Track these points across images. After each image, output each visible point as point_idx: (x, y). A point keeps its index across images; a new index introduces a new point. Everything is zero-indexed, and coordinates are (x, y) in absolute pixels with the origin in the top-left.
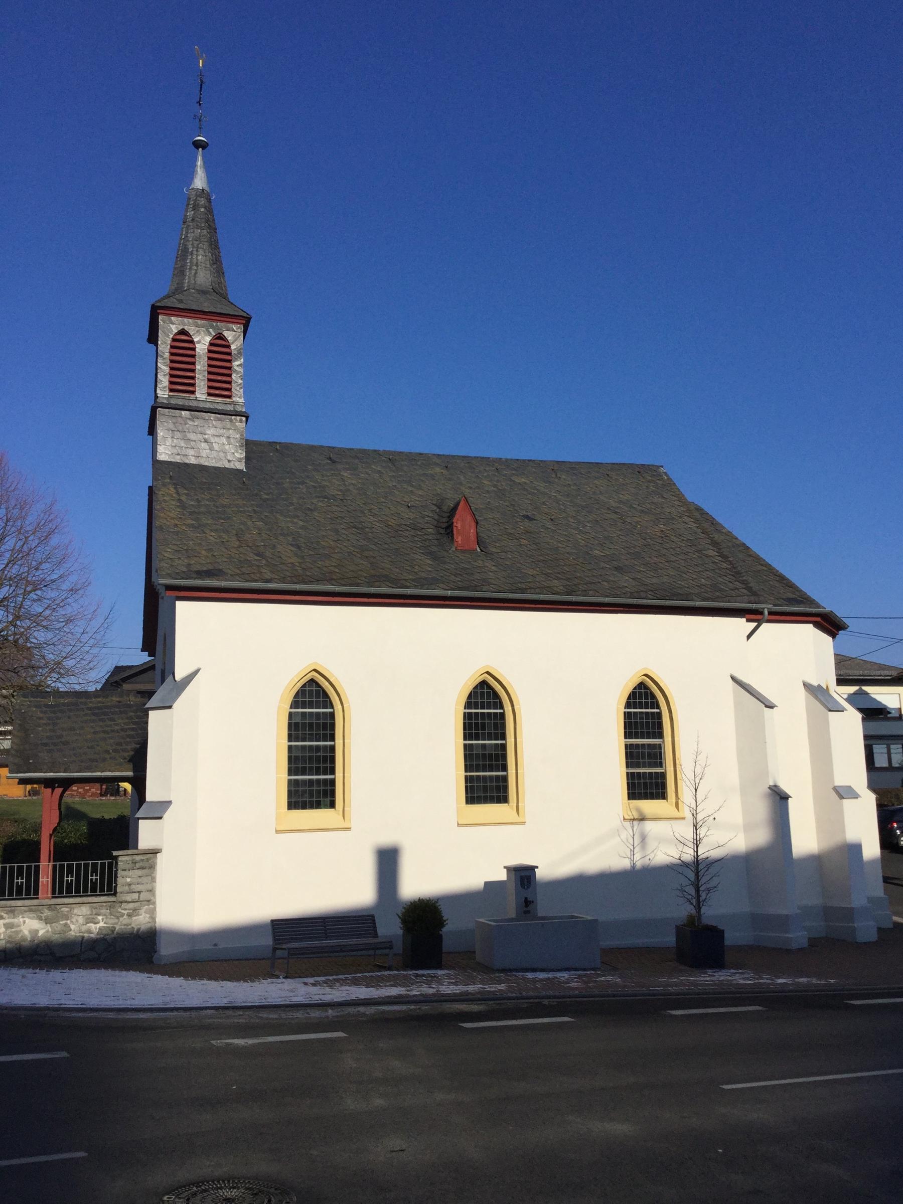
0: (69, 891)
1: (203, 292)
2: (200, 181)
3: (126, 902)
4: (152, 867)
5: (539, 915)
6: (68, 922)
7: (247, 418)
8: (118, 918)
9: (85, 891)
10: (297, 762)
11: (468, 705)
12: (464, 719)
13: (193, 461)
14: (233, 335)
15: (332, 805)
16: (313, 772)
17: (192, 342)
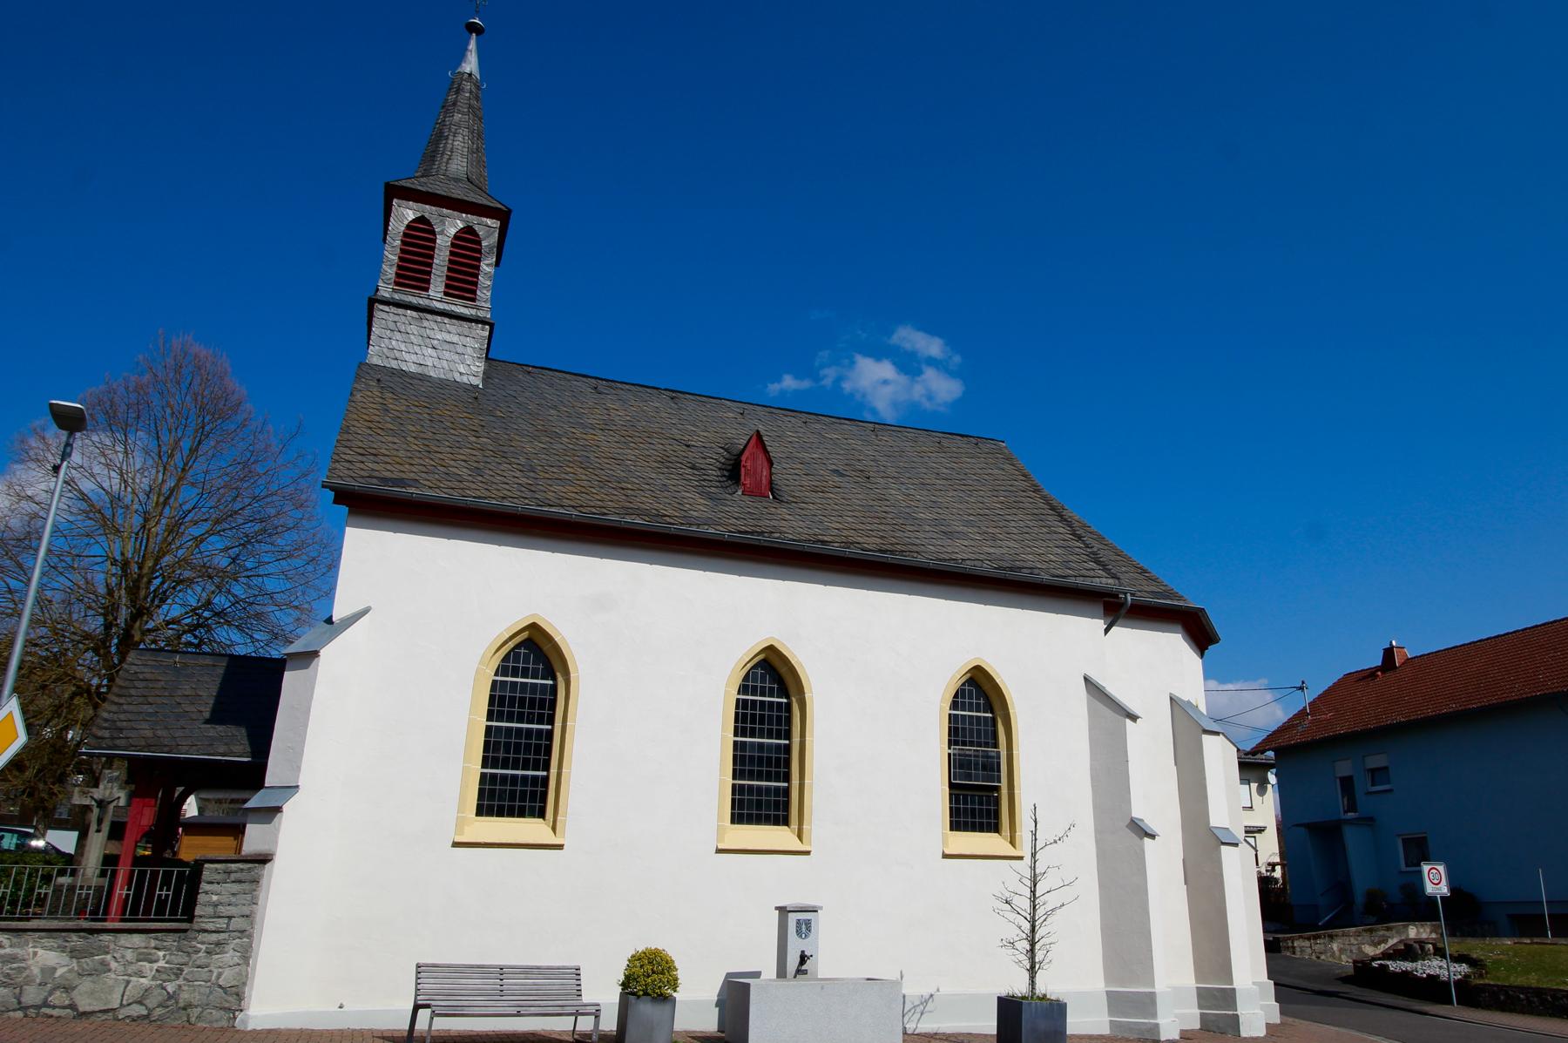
0: (161, 910)
1: (457, 180)
2: (471, 65)
3: (206, 931)
4: (256, 882)
6: (109, 957)
7: (492, 326)
8: (189, 954)
9: (147, 911)
10: (496, 749)
11: (743, 689)
12: (737, 707)
13: (413, 369)
14: (487, 229)
16: (519, 762)
17: (433, 233)
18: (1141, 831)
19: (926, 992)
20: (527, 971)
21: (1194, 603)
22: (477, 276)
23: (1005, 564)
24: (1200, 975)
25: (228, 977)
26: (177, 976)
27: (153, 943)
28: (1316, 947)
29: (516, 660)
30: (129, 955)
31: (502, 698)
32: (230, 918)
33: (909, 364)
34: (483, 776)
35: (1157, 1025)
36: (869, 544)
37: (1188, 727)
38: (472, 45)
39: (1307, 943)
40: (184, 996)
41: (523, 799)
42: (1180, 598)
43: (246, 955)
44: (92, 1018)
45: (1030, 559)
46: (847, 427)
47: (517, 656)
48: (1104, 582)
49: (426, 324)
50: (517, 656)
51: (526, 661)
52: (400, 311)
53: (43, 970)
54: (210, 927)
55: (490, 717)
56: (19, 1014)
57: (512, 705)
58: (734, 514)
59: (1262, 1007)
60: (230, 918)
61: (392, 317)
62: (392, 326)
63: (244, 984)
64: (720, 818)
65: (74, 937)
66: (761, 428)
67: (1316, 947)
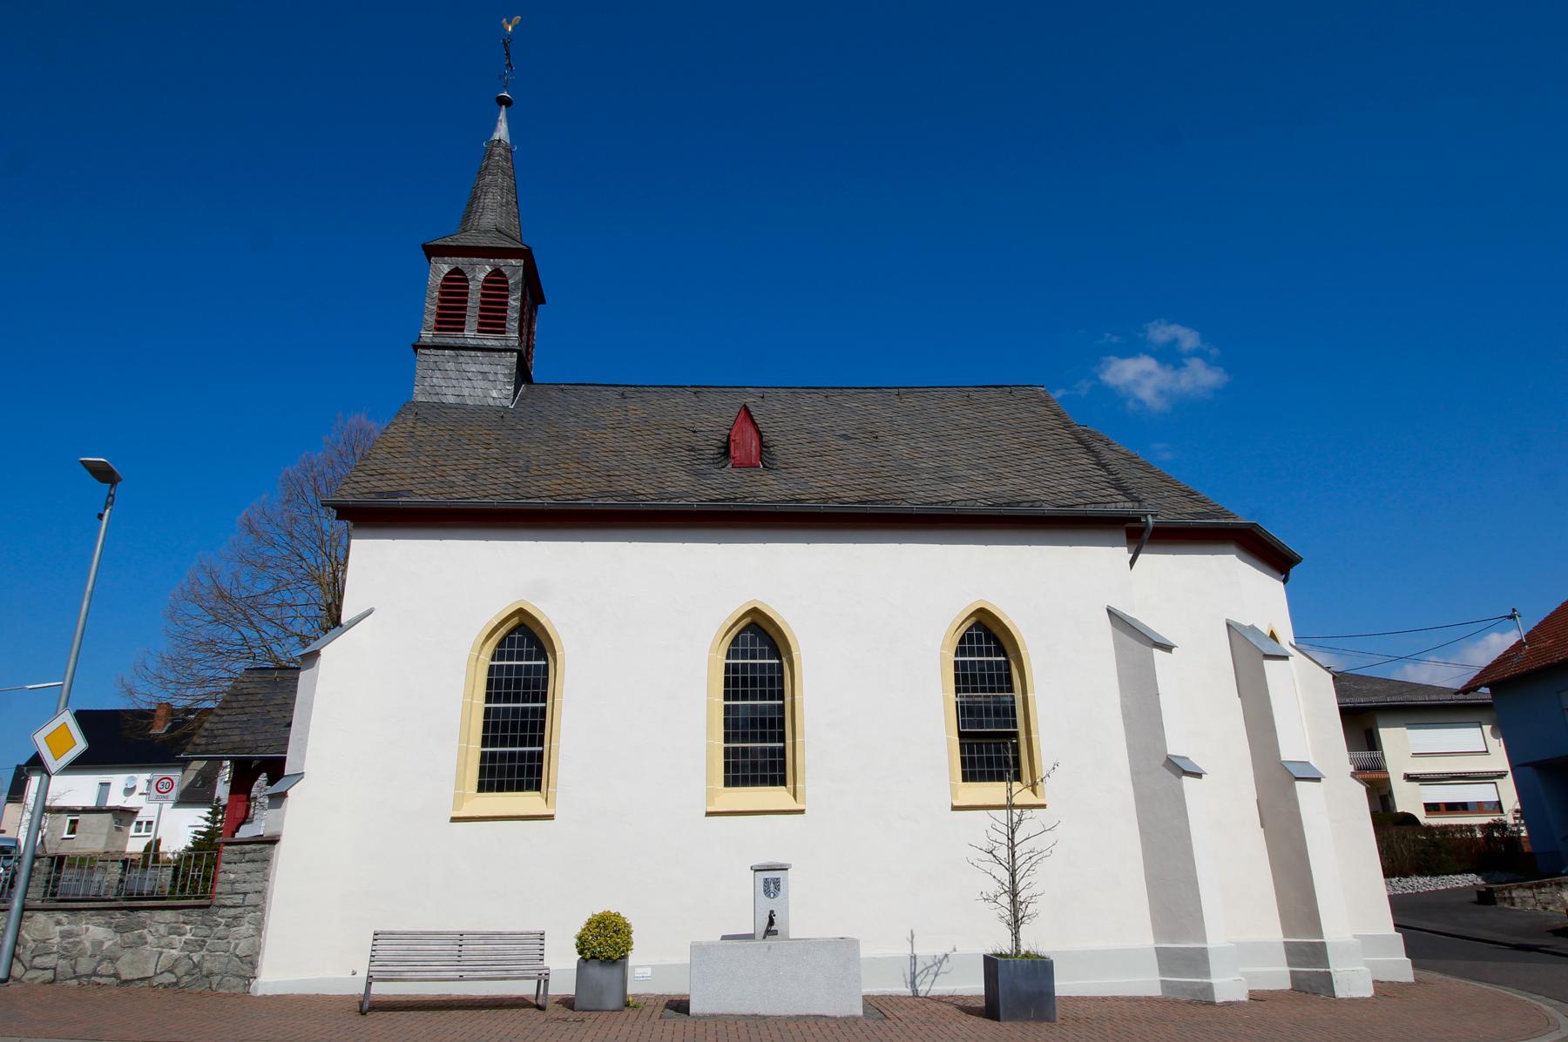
1: (486, 232)
2: (502, 132)
4: (267, 860)
5: (109, 815)
8: (211, 928)
9: (183, 890)
10: (495, 729)
13: (451, 400)
15: (538, 788)
16: (514, 747)
17: (466, 280)
18: (1180, 769)
19: (940, 953)
20: (486, 937)
21: (1243, 519)
22: (505, 311)
23: (1001, 501)
24: (1287, 929)
25: (243, 948)
26: (202, 947)
27: (182, 918)
28: (1542, 897)
29: (511, 645)
30: (162, 929)
31: (499, 682)
32: (245, 894)
33: (1170, 356)
34: (483, 755)
35: (1210, 985)
36: (850, 495)
37: (1250, 651)
38: (502, 116)
39: (1528, 893)
40: (207, 965)
41: (521, 774)
42: (1230, 515)
43: (259, 927)
44: (133, 985)
45: (1035, 493)
46: (871, 394)
47: (512, 641)
48: (1123, 506)
49: (461, 359)
50: (512, 641)
51: (520, 645)
52: (439, 352)
53: (93, 943)
54: (228, 902)
55: (488, 699)
56: (74, 982)
57: (508, 686)
58: (722, 486)
59: (1367, 964)
60: (245, 894)
61: (433, 359)
62: (432, 366)
63: (258, 954)
64: (709, 780)
65: (118, 914)
66: (749, 401)
67: (1542, 897)
